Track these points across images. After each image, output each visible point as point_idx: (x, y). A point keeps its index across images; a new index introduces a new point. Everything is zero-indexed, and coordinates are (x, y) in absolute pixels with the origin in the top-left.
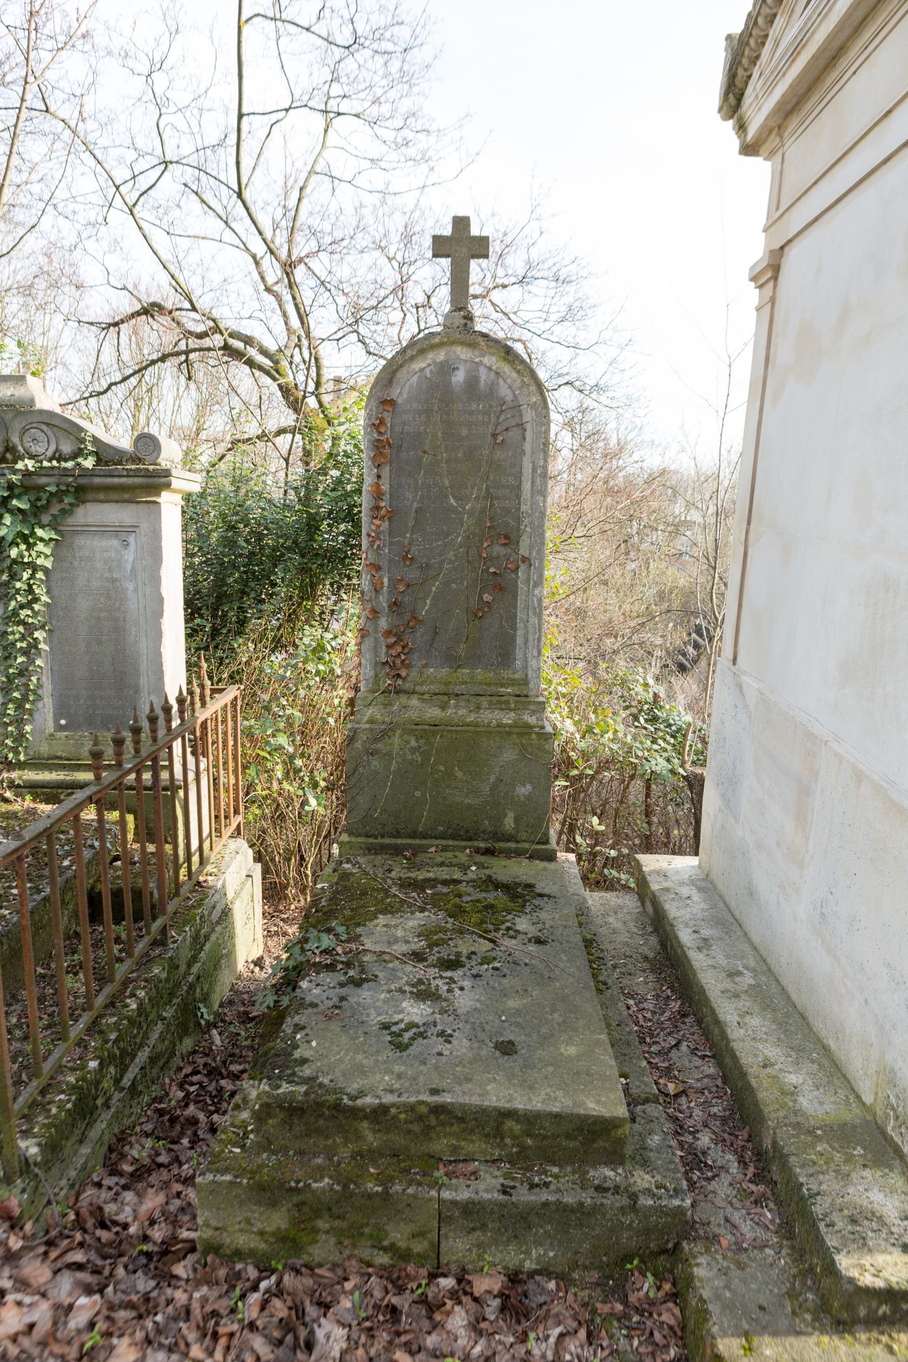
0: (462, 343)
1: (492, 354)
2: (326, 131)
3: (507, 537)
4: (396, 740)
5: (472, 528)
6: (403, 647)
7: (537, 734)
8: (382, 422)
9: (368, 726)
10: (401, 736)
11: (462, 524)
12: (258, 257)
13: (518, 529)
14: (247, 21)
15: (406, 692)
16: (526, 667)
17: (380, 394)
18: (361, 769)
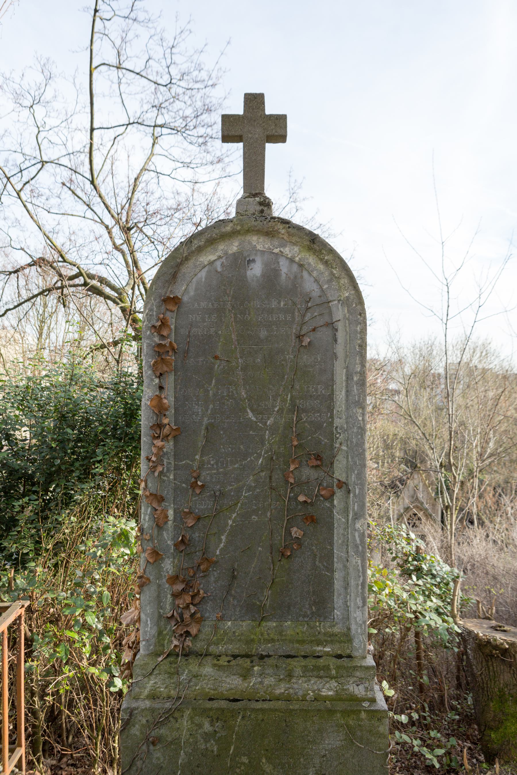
0: (259, 232)
1: (294, 244)
2: (153, 145)
3: (318, 457)
4: (185, 723)
5: (275, 447)
6: (193, 597)
7: (367, 712)
8: (164, 323)
9: (148, 703)
10: (191, 718)
11: (263, 444)
12: (110, 227)
13: (332, 447)
14: (96, 68)
15: (199, 655)
16: (348, 619)
17: (162, 292)
18: (139, 763)
